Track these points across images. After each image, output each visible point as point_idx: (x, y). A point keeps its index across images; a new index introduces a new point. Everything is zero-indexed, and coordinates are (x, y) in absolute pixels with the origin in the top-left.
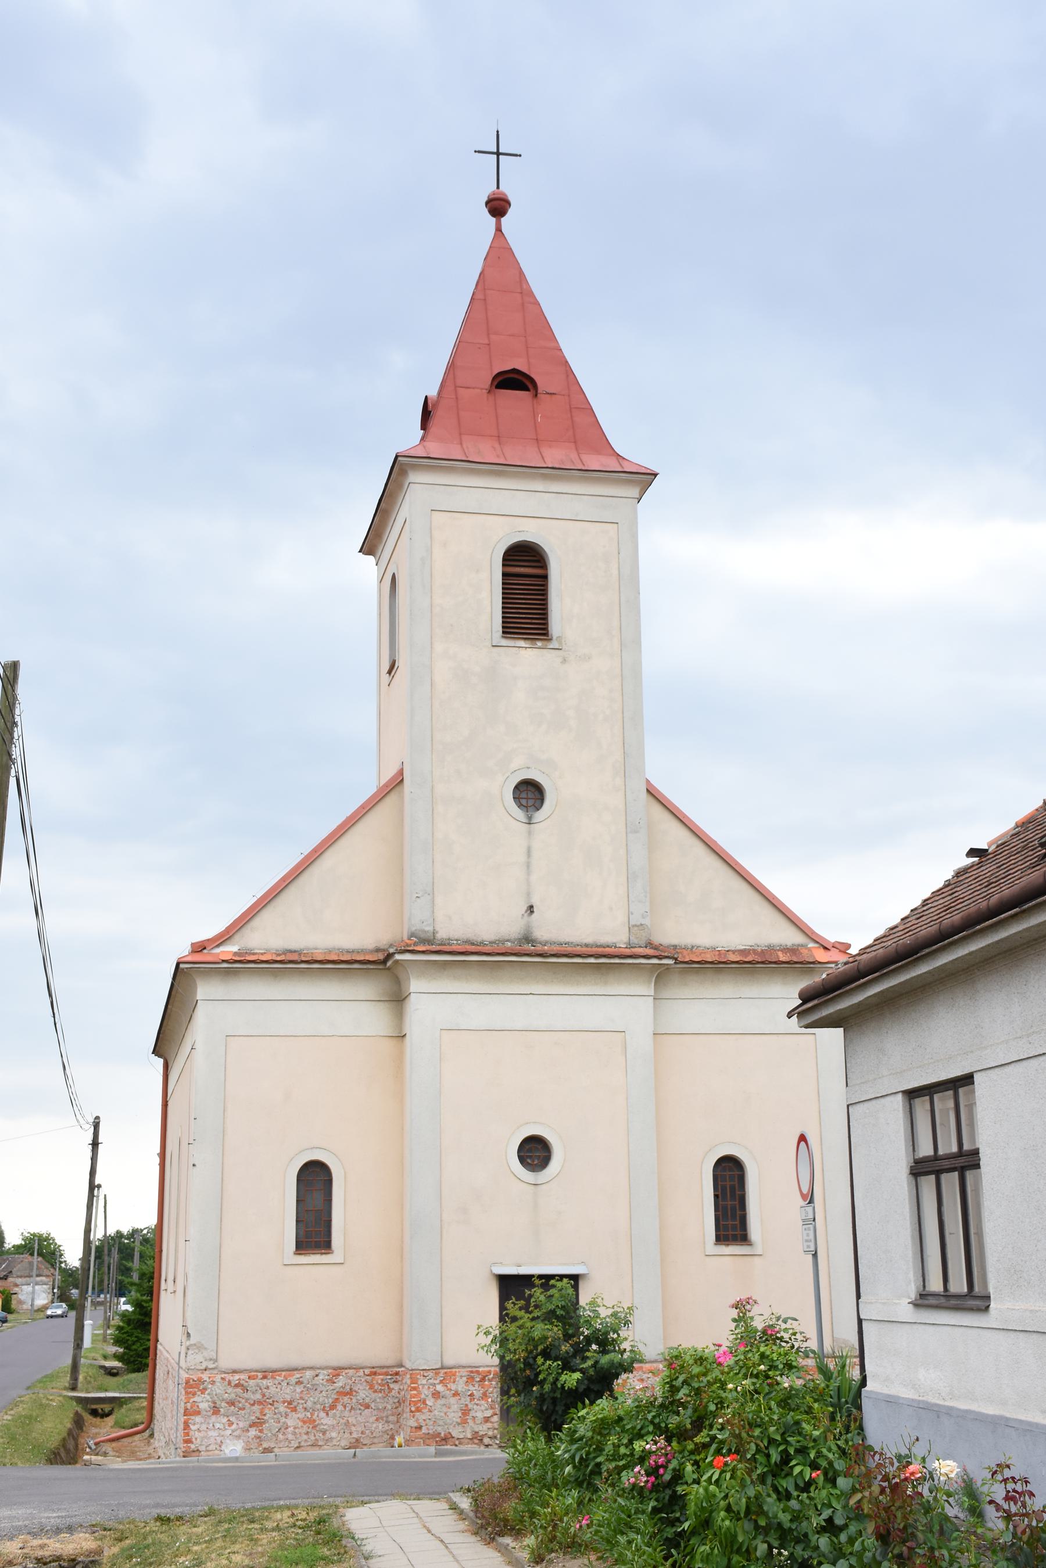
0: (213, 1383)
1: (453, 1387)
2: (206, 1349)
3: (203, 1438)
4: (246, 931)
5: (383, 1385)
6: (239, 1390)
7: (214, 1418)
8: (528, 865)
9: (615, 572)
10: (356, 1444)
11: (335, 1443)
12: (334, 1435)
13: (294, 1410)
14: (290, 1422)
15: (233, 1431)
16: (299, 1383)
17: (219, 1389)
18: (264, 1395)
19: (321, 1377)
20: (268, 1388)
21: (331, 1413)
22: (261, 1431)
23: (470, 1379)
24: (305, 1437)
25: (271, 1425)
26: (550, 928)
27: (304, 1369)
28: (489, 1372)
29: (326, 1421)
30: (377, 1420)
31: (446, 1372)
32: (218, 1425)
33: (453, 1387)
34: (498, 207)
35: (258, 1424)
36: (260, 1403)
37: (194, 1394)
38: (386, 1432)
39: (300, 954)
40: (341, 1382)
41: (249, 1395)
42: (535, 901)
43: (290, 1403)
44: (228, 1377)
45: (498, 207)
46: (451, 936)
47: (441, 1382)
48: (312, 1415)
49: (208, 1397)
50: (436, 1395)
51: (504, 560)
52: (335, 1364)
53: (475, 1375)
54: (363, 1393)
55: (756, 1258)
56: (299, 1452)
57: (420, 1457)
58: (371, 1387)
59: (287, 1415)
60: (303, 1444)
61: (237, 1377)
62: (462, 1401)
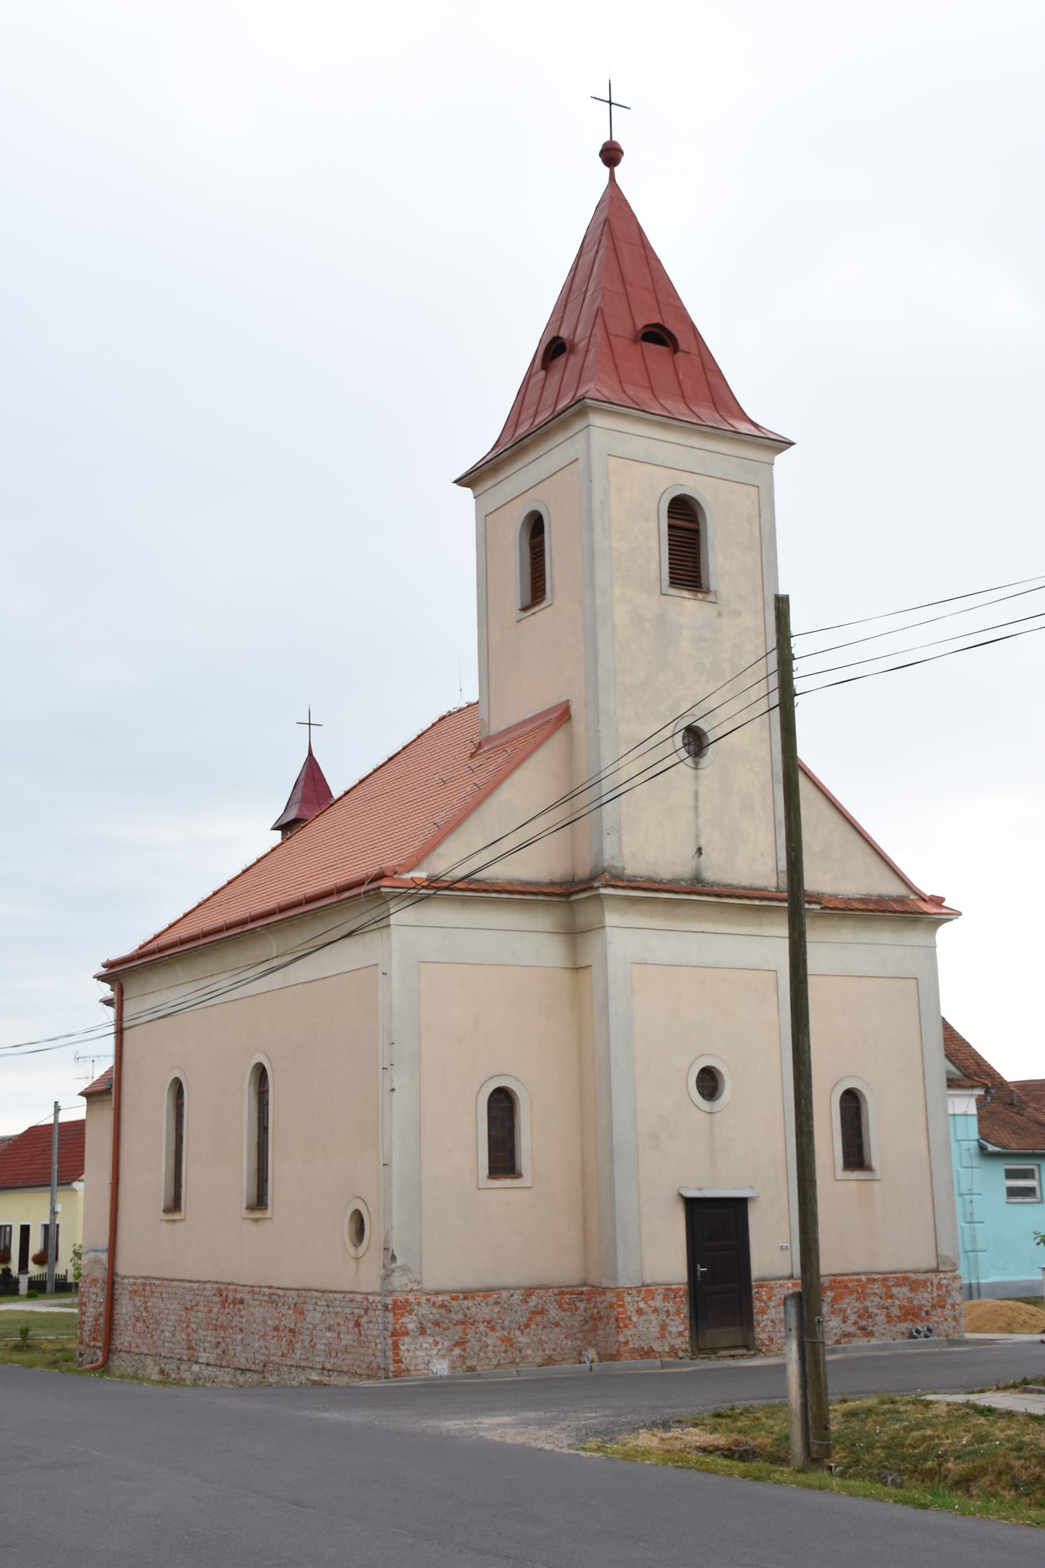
0: (419, 1304)
1: (652, 1304)
2: (411, 1271)
3: (411, 1358)
4: (433, 857)
5: (570, 1304)
6: (443, 1311)
7: (421, 1339)
8: (696, 809)
9: (757, 533)
10: (549, 1361)
11: (530, 1359)
12: (529, 1352)
13: (493, 1329)
14: (490, 1341)
15: (439, 1350)
16: (496, 1303)
17: (425, 1310)
18: (465, 1315)
19: (516, 1297)
20: (468, 1308)
21: (526, 1332)
22: (464, 1350)
23: (666, 1297)
24: (504, 1355)
25: (473, 1345)
26: (714, 872)
27: (499, 1289)
28: (680, 1289)
29: (522, 1339)
30: (566, 1337)
31: (646, 1290)
32: (425, 1345)
33: (652, 1304)
34: (611, 155)
35: (461, 1343)
36: (462, 1323)
37: (402, 1315)
38: (574, 1349)
39: (712, 886)
40: (533, 1301)
41: (454, 1316)
42: (703, 843)
43: (489, 1322)
44: (433, 1298)
45: (611, 155)
46: (637, 873)
47: (643, 1299)
48: (509, 1333)
49: (415, 1318)
50: (640, 1312)
51: (669, 512)
52: (527, 1284)
53: (669, 1292)
54: (554, 1313)
55: (875, 1183)
56: (499, 1370)
57: (648, 1369)
58: (560, 1306)
59: (486, 1335)
60: (502, 1361)
61: (440, 1298)
62: (660, 1317)
